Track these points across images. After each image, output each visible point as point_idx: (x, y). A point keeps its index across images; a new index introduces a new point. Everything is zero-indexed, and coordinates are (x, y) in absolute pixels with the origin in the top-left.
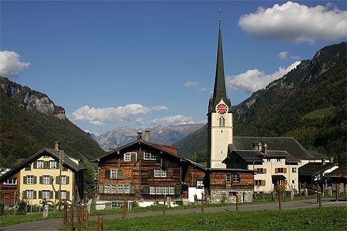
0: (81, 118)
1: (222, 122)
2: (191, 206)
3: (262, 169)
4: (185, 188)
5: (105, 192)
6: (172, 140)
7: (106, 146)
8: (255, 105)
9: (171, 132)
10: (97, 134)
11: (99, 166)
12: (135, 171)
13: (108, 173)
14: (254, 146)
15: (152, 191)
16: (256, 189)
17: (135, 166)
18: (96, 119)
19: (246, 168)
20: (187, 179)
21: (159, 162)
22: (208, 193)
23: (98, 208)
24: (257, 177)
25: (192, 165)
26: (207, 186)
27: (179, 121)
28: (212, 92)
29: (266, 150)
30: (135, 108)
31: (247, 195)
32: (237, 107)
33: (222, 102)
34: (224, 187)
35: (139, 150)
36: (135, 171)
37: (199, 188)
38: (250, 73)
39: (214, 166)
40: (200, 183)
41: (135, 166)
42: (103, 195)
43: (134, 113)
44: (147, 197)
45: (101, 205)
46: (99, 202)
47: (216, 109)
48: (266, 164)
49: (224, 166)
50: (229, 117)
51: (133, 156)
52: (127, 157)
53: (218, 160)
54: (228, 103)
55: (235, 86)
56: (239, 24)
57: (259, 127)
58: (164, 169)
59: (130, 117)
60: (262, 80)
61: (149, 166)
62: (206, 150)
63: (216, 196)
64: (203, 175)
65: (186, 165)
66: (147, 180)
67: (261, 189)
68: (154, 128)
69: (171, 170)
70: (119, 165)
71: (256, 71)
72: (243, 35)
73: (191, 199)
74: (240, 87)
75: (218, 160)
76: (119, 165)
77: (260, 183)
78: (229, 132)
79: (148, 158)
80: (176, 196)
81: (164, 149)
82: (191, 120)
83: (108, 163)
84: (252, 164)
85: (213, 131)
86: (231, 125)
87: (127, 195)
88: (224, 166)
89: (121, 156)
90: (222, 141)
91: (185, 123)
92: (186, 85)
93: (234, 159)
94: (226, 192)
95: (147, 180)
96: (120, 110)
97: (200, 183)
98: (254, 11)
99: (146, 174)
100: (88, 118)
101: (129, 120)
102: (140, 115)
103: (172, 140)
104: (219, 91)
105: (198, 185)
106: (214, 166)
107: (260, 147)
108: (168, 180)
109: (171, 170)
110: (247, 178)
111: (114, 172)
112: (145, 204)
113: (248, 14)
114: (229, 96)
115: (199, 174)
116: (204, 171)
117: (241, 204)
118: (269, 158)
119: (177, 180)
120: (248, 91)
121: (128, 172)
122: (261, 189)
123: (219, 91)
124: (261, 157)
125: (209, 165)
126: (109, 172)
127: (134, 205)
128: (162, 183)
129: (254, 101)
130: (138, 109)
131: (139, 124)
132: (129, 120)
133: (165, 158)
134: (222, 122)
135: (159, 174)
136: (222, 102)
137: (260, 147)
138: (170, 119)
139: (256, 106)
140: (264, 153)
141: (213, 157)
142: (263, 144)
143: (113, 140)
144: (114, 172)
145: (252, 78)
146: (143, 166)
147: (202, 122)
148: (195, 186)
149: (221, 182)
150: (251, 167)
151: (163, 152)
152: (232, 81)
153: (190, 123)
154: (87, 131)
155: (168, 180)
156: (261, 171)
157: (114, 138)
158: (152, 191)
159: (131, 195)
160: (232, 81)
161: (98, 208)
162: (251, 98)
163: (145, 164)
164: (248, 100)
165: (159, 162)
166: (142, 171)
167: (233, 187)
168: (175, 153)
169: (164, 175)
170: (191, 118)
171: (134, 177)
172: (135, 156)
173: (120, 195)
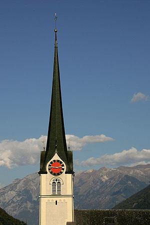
1: (57, 191)
9: (124, 180)
33: (56, 157)
91: (144, 163)
134: (57, 191)
136: (56, 157)
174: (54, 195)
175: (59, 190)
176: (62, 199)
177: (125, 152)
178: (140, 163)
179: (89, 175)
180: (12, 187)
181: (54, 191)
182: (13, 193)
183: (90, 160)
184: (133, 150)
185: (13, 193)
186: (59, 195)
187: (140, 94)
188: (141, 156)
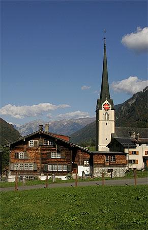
0: (5, 113)
1: (107, 117)
2: (82, 179)
3: (135, 152)
4: (75, 166)
5: (15, 169)
6: (73, 129)
7: (24, 133)
8: (135, 103)
9: (73, 125)
10: (18, 125)
11: (10, 150)
12: (37, 153)
13: (17, 155)
14: (130, 134)
15: (50, 168)
16: (130, 166)
17: (37, 150)
18: (16, 114)
19: (123, 151)
20: (76, 159)
21: (55, 147)
22: (92, 170)
23: (10, 181)
24: (131, 157)
25: (80, 149)
26: (91, 164)
27: (78, 116)
28: (99, 94)
29: (138, 138)
30: (45, 106)
31: (119, 172)
32: (120, 106)
33: (106, 102)
34: (103, 165)
35: (40, 138)
36: (37, 153)
37: (86, 166)
38: (131, 79)
39: (101, 149)
40: (86, 162)
41: (37, 150)
42: (13, 171)
43: (44, 109)
44: (46, 172)
45: (12, 179)
46: (11, 177)
47: (102, 106)
48: (138, 148)
49: (108, 150)
50: (112, 113)
51: (35, 143)
52: (31, 143)
53: (103, 148)
54: (111, 102)
55: (118, 89)
56: (122, 41)
57: (138, 120)
58: (58, 152)
59: (42, 113)
60: (139, 84)
61: (48, 150)
62: (95, 138)
63: (98, 172)
64: (89, 156)
65: (75, 150)
66: (46, 160)
67: (134, 166)
68: (61, 120)
69: (64, 153)
70: (25, 149)
71: (136, 78)
72: (125, 49)
73: (80, 174)
74: (123, 90)
75: (103, 148)
76: (25, 149)
77: (133, 162)
78: (112, 124)
79: (47, 144)
80: (68, 172)
81: (58, 137)
82: (87, 115)
83: (18, 148)
84: (127, 148)
85: (100, 123)
86: (113, 119)
87: (32, 171)
88: (108, 150)
89: (26, 143)
90: (107, 131)
91: (83, 117)
92: (82, 88)
93: (116, 145)
94: (105, 169)
95: (46, 160)
96: (34, 108)
97: (86, 162)
98: (134, 31)
99: (46, 156)
100: (10, 113)
101: (42, 115)
102: (50, 111)
103: (73, 129)
104: (105, 94)
105: (85, 164)
106: (101, 149)
107: (134, 136)
108: (62, 160)
109: (64, 153)
110: (121, 159)
111: (21, 155)
112: (43, 178)
113: (130, 33)
114: (112, 97)
115: (85, 155)
116: (89, 153)
117: (107, 179)
118: (140, 144)
119: (68, 160)
120: (129, 93)
121: (32, 155)
122: (134, 166)
123: (105, 94)
124: (135, 143)
125: (97, 149)
126: (18, 154)
127: (36, 179)
128: (57, 162)
129: (134, 101)
130: (48, 106)
131: (49, 118)
132: (42, 115)
133: (60, 144)
134: (107, 117)
135: (55, 156)
136: (106, 102)
137: (134, 136)
138: (72, 114)
139: (135, 104)
140: (137, 139)
141: (100, 143)
142: (136, 133)
143: (55, 125)
144: (21, 155)
145: (132, 83)
146: (43, 150)
147: (93, 117)
148: (83, 164)
149: (102, 162)
150: (126, 151)
151: (58, 139)
152: (117, 86)
153: (87, 116)
154: (10, 123)
155: (62, 160)
156: (134, 153)
157: (30, 128)
158: (50, 168)
159: (34, 171)
160: (117, 86)
161: (10, 181)
162: (132, 98)
163: (44, 148)
164: (130, 100)
165: (55, 147)
166: (42, 154)
167: (110, 165)
168: (67, 140)
169: (59, 156)
170: (87, 113)
171: (37, 158)
172: (37, 143)
173: (26, 171)
174: (105, 120)
175: (108, 118)
176: (110, 122)
177: (76, 112)
178: (80, 117)
179: (58, 122)
180: (24, 127)
181: (105, 118)
182: (25, 129)
183: (60, 115)
184: (79, 112)
185: (25, 129)
186: (108, 120)
187: (85, 86)
188: (82, 115)
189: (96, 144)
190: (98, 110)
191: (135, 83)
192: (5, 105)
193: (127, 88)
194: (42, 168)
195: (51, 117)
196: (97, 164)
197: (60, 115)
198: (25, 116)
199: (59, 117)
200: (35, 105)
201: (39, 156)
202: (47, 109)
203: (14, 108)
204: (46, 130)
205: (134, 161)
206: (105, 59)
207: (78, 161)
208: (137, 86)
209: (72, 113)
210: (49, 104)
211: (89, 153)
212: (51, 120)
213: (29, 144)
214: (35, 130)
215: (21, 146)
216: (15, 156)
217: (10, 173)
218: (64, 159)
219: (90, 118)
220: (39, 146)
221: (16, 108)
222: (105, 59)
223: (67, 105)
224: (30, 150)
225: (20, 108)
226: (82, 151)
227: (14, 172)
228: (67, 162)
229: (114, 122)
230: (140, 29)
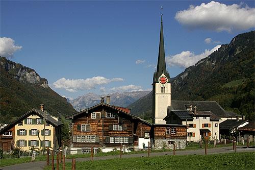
0: (59, 87)
1: (163, 90)
2: (141, 151)
3: (192, 125)
4: (136, 139)
5: (78, 141)
6: (127, 103)
7: (78, 108)
8: (187, 77)
9: (126, 97)
10: (71, 99)
12: (99, 126)
14: (186, 107)
15: (112, 141)
16: (188, 139)
17: (99, 122)
18: (71, 88)
19: (181, 124)
20: (137, 132)
21: (117, 119)
22: (153, 142)
23: (72, 153)
24: (189, 130)
25: (141, 121)
26: (152, 137)
27: (131, 89)
28: (156, 68)
30: (99, 79)
31: (181, 144)
32: (174, 79)
33: (163, 75)
34: (164, 137)
36: (99, 126)
37: (146, 138)
38: (184, 53)
39: (157, 122)
40: (147, 135)
42: (76, 143)
44: (108, 145)
45: (74, 151)
47: (159, 80)
48: (195, 121)
49: (165, 123)
50: (168, 86)
51: (98, 115)
52: (93, 116)
53: (160, 118)
55: (172, 63)
56: (190, 6)
57: (190, 94)
58: (120, 124)
59: (96, 86)
60: (192, 59)
61: (110, 122)
63: (159, 144)
64: (149, 129)
65: (137, 122)
66: (108, 132)
67: (192, 139)
69: (126, 125)
73: (141, 147)
74: (177, 64)
75: (160, 118)
77: (191, 134)
78: (169, 97)
79: (109, 116)
80: (129, 144)
84: (185, 120)
85: (157, 96)
86: (170, 92)
88: (165, 123)
89: (89, 115)
90: (163, 104)
91: (136, 91)
93: (172, 117)
94: (166, 141)
95: (108, 132)
97: (147, 135)
98: (187, 8)
99: (107, 128)
102: (103, 85)
103: (127, 103)
104: (161, 67)
105: (146, 136)
106: (157, 122)
107: (191, 109)
109: (126, 125)
110: (183, 131)
111: (84, 127)
112: (106, 150)
114: (168, 71)
115: (146, 128)
116: (150, 126)
117: (177, 150)
118: (197, 117)
119: (130, 133)
120: (182, 67)
121: (94, 127)
122: (192, 139)
123: (161, 67)
124: (192, 116)
125: (154, 122)
126: (80, 126)
127: (99, 151)
128: (119, 135)
129: (186, 75)
130: (102, 80)
131: (102, 91)
133: (121, 116)
134: (163, 90)
135: (117, 128)
136: (163, 75)
137: (191, 109)
138: (125, 88)
142: (193, 106)
143: (83, 103)
144: (84, 127)
145: (185, 57)
146: (105, 122)
147: (149, 90)
148: (143, 137)
149: (162, 134)
150: (184, 123)
151: (120, 112)
152: (171, 60)
153: (140, 90)
156: (192, 126)
158: (112, 141)
159: (97, 144)
160: (171, 60)
161: (72, 153)
162: (185, 72)
163: (107, 121)
164: (182, 74)
165: (117, 119)
166: (104, 126)
167: (171, 137)
168: (129, 113)
169: (120, 128)
170: (140, 87)
172: (99, 115)
173: (88, 143)
178: (132, 91)
180: (77, 100)
182: (78, 102)
183: (114, 89)
185: (78, 102)
189: (153, 116)
190: (155, 83)
191: (189, 58)
192: (59, 79)
193: (181, 62)
194: (104, 141)
195: (105, 90)
196: (158, 136)
197: (114, 89)
198: (78, 89)
199: (113, 91)
200: (88, 79)
201: (101, 128)
202: (100, 83)
203: (68, 82)
204: (108, 102)
205: (191, 133)
206: (161, 34)
207: (139, 134)
208: (191, 60)
209: (125, 87)
210: (102, 78)
211: (150, 126)
212: (105, 93)
213: (92, 117)
214: (99, 103)
215: (83, 118)
216: (78, 128)
217: (72, 145)
218: (126, 131)
219: (143, 92)
220: (101, 118)
221: (70, 81)
222: (161, 34)
223: (120, 79)
224: (93, 122)
225: (74, 81)
226: (143, 124)
227: (76, 144)
228: (128, 134)
229: (170, 95)
230: (193, 7)
